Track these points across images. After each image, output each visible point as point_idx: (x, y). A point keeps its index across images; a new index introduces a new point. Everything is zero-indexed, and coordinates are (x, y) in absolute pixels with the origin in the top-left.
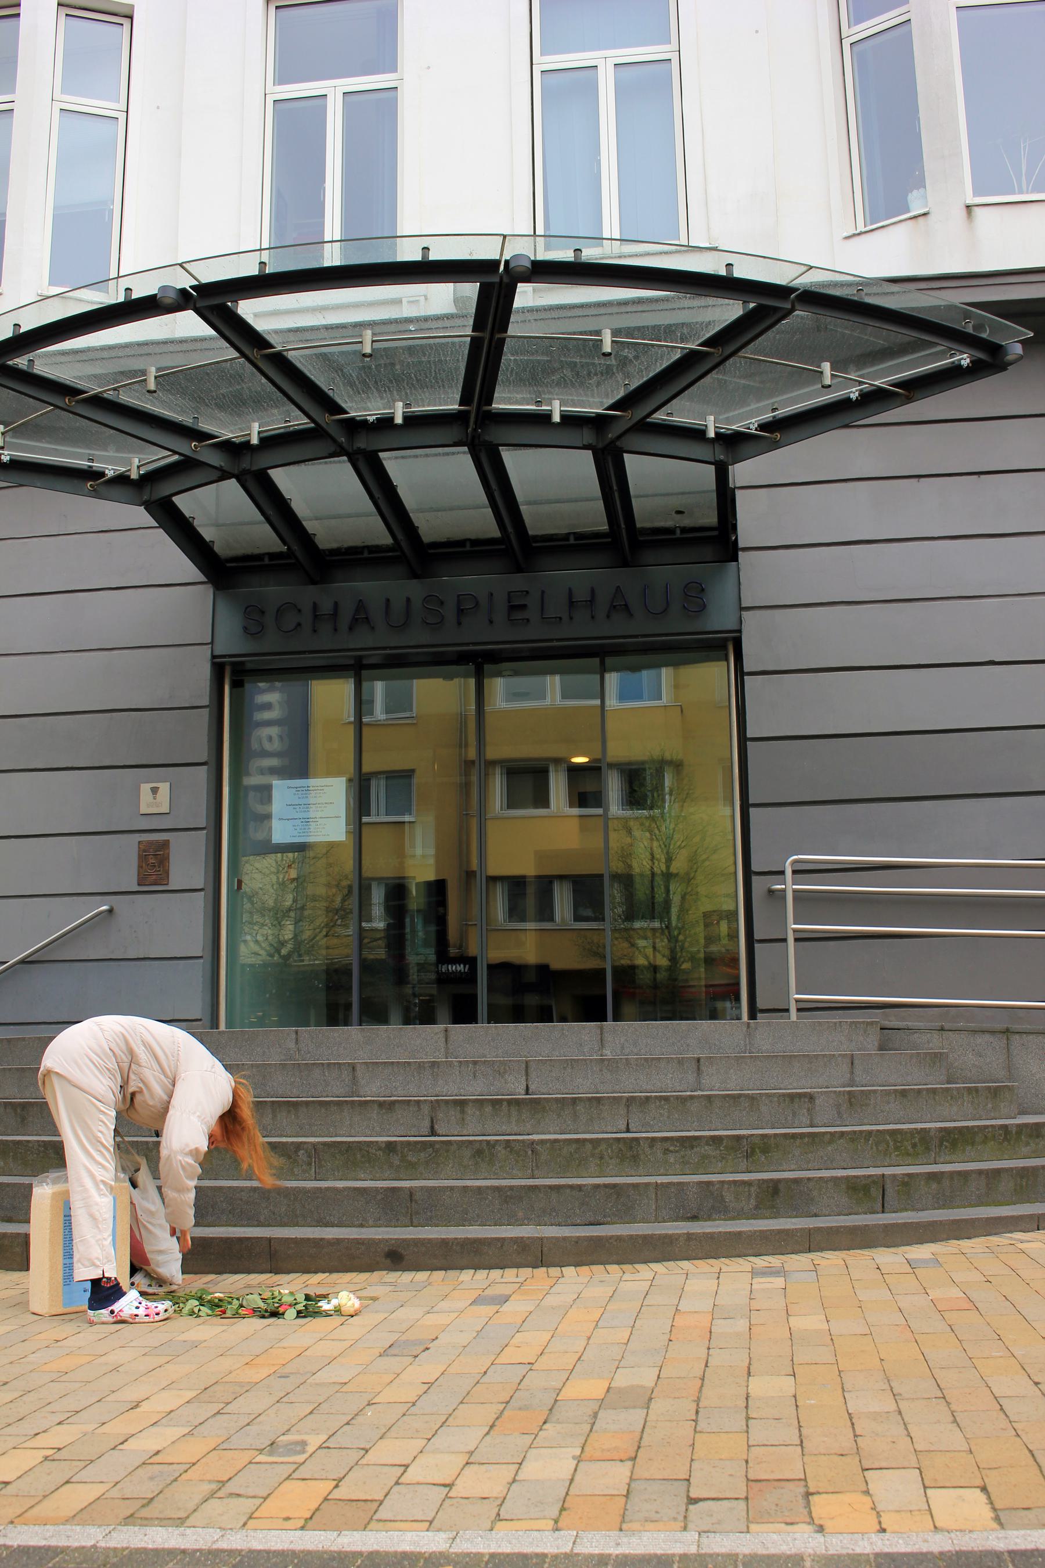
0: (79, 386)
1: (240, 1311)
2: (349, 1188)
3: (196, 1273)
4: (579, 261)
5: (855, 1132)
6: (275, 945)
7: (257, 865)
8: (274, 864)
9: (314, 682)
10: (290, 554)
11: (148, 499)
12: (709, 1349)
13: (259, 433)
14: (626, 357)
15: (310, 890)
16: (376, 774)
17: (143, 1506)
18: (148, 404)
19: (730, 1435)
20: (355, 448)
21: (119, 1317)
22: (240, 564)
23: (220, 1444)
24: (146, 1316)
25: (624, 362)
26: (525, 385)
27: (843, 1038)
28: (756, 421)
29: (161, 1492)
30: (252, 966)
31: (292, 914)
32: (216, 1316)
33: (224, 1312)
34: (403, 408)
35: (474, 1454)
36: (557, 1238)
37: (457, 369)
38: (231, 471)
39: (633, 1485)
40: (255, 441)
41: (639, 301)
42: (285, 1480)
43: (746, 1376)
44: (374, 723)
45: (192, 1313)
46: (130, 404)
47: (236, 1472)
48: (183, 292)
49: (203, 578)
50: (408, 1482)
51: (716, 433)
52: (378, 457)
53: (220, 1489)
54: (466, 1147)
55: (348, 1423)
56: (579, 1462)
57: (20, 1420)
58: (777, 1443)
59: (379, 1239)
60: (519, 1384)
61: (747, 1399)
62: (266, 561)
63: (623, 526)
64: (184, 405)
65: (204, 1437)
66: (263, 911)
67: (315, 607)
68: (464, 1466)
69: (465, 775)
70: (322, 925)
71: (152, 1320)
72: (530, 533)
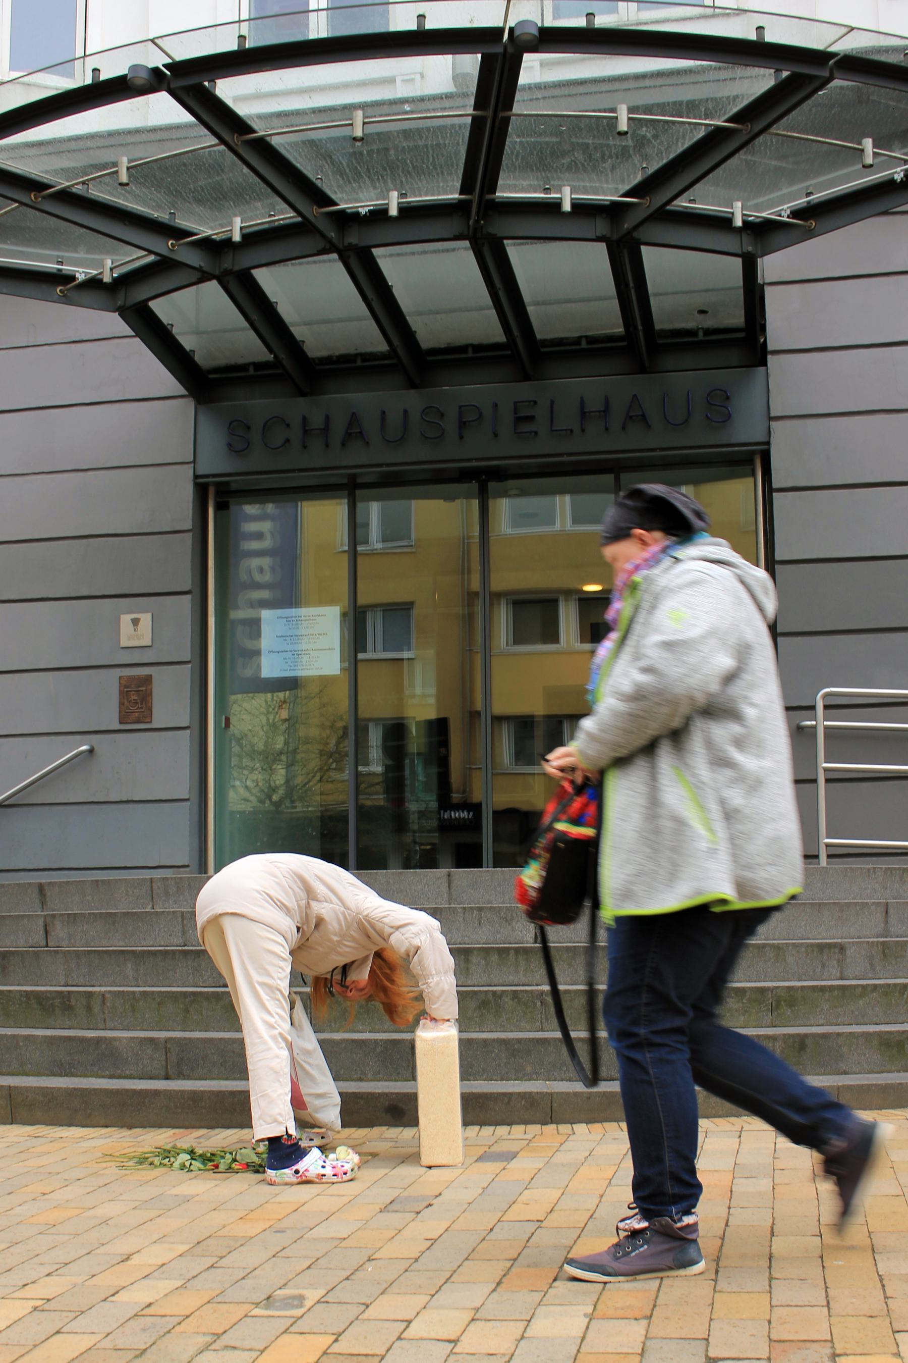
0: (45, 181)
1: (233, 1165)
2: (347, 1040)
3: (187, 1128)
4: (591, 26)
5: (889, 985)
6: (266, 790)
7: (245, 705)
8: (264, 704)
9: (305, 503)
10: (277, 363)
11: (123, 304)
12: (729, 1208)
13: (241, 228)
14: (644, 137)
15: (302, 732)
16: (373, 607)
17: (136, 1357)
18: (119, 198)
19: (752, 1295)
20: (346, 244)
21: (304, 1178)
22: (224, 376)
23: (214, 1298)
24: (334, 1175)
25: (641, 143)
26: (532, 170)
27: (877, 885)
28: (788, 208)
29: (154, 1344)
30: (241, 813)
31: (283, 758)
32: (209, 1170)
33: (217, 1167)
34: (398, 198)
35: (480, 1311)
36: (568, 1094)
37: (457, 153)
38: (212, 272)
39: (648, 1343)
40: (237, 237)
41: (660, 74)
42: (282, 1333)
43: (769, 1236)
44: (369, 552)
45: (182, 1167)
46: (100, 200)
47: (231, 1325)
48: (156, 71)
49: (183, 391)
50: (412, 1337)
51: (744, 222)
52: (371, 254)
53: (215, 1341)
54: (471, 998)
55: (347, 1279)
56: (591, 1319)
57: (8, 1271)
58: (802, 1304)
59: (379, 1093)
60: (528, 1241)
61: (770, 1259)
62: (251, 372)
63: (640, 328)
64: (160, 199)
65: (198, 1290)
66: (253, 754)
67: (305, 420)
68: (470, 1323)
69: (468, 605)
70: (316, 769)
71: (340, 1180)
72: (539, 336)
